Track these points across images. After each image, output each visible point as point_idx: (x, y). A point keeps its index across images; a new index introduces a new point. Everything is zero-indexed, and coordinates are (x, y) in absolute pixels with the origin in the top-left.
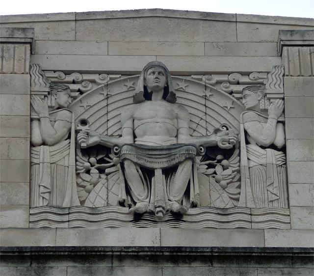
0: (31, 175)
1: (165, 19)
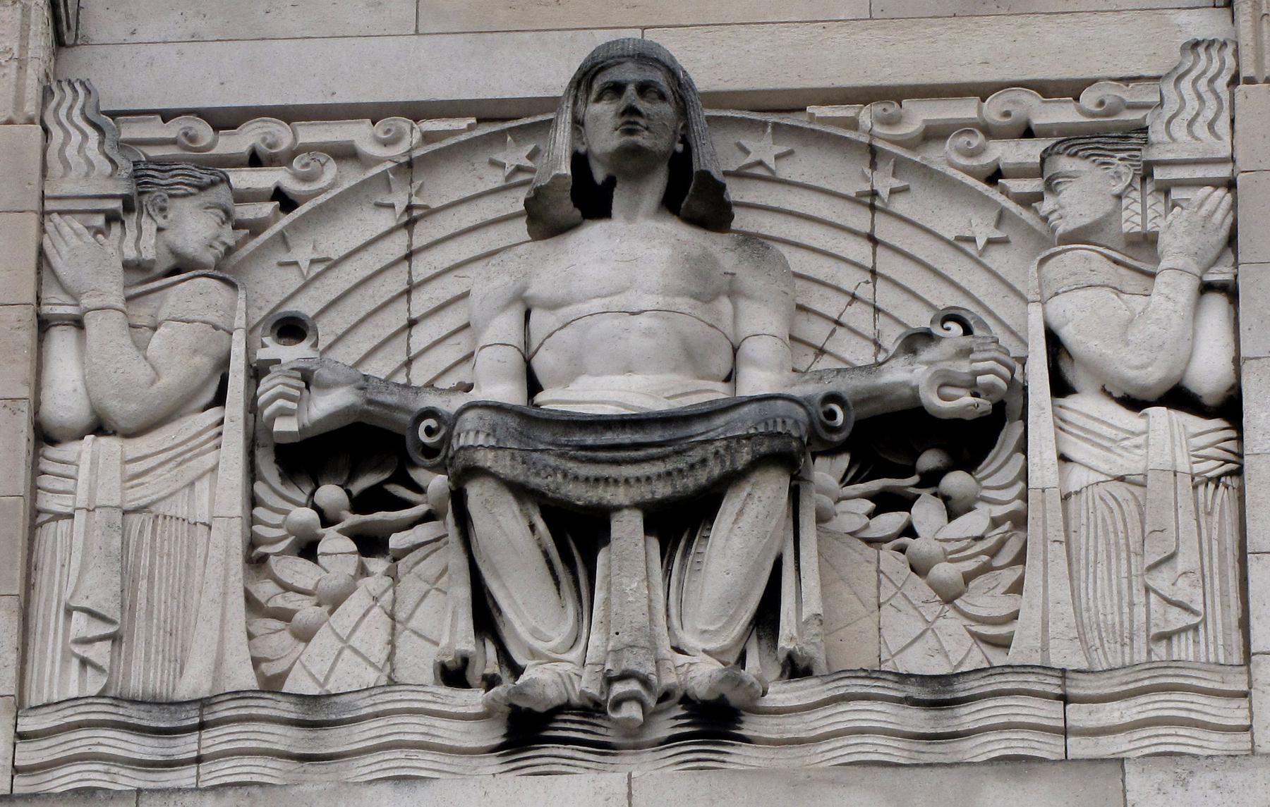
0: (30, 568)
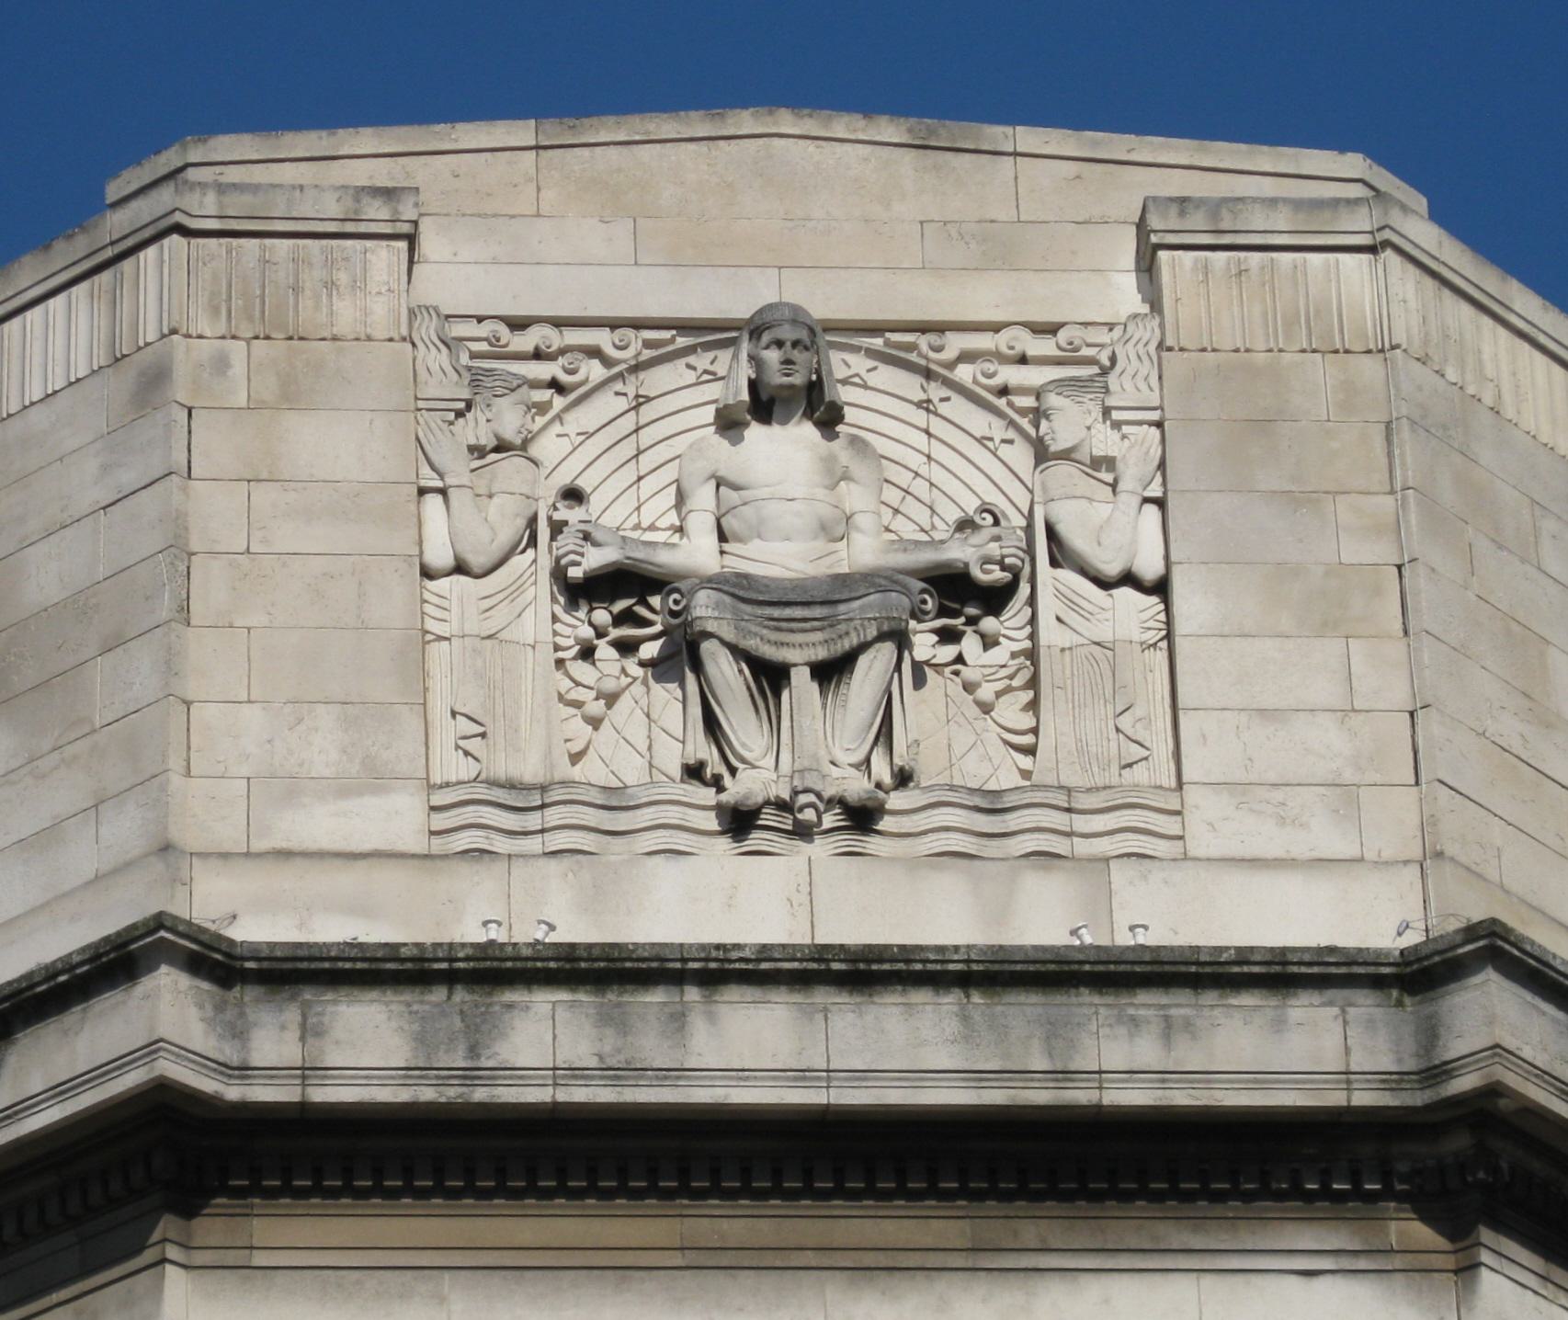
1: (801, 142)
